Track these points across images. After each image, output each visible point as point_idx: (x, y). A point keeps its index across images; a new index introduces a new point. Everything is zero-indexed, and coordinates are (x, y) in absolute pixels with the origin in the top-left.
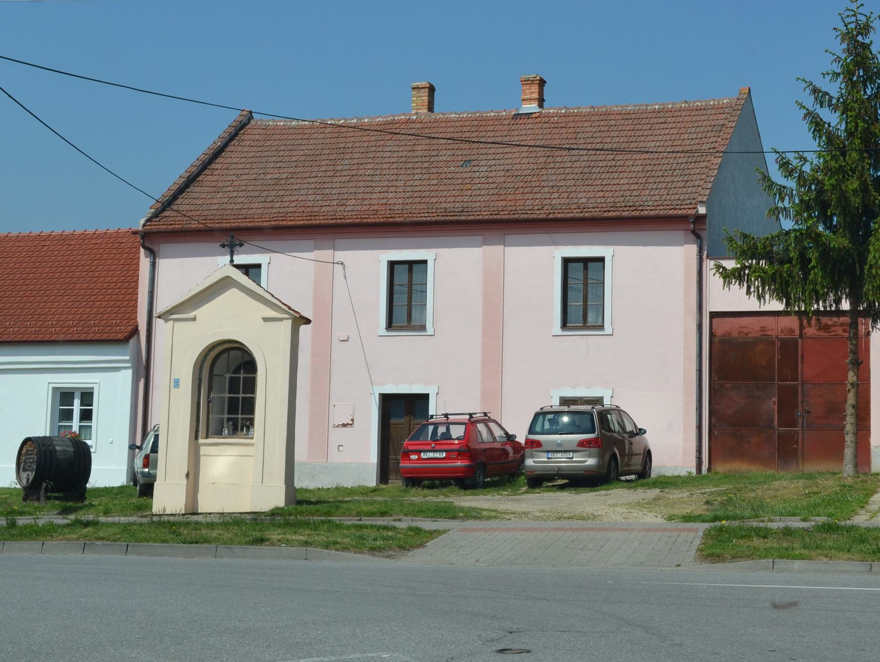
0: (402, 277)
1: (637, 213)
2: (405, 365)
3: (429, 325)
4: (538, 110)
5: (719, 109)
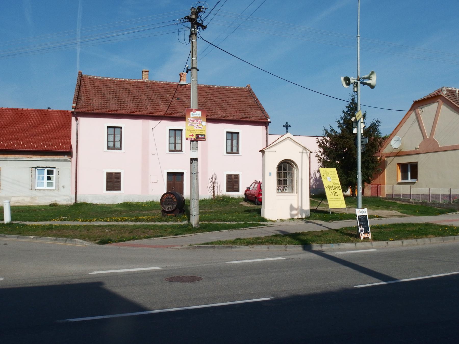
1: (250, 120)
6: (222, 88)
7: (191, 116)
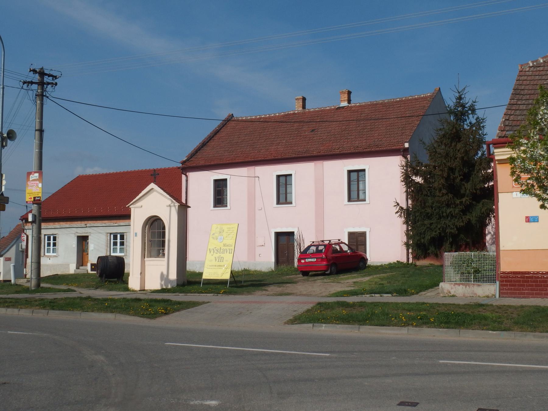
0: (354, 176)
1: (378, 149)
2: (285, 219)
3: (293, 202)
4: (347, 105)
5: (425, 98)
6: (397, 102)
7: (31, 179)
